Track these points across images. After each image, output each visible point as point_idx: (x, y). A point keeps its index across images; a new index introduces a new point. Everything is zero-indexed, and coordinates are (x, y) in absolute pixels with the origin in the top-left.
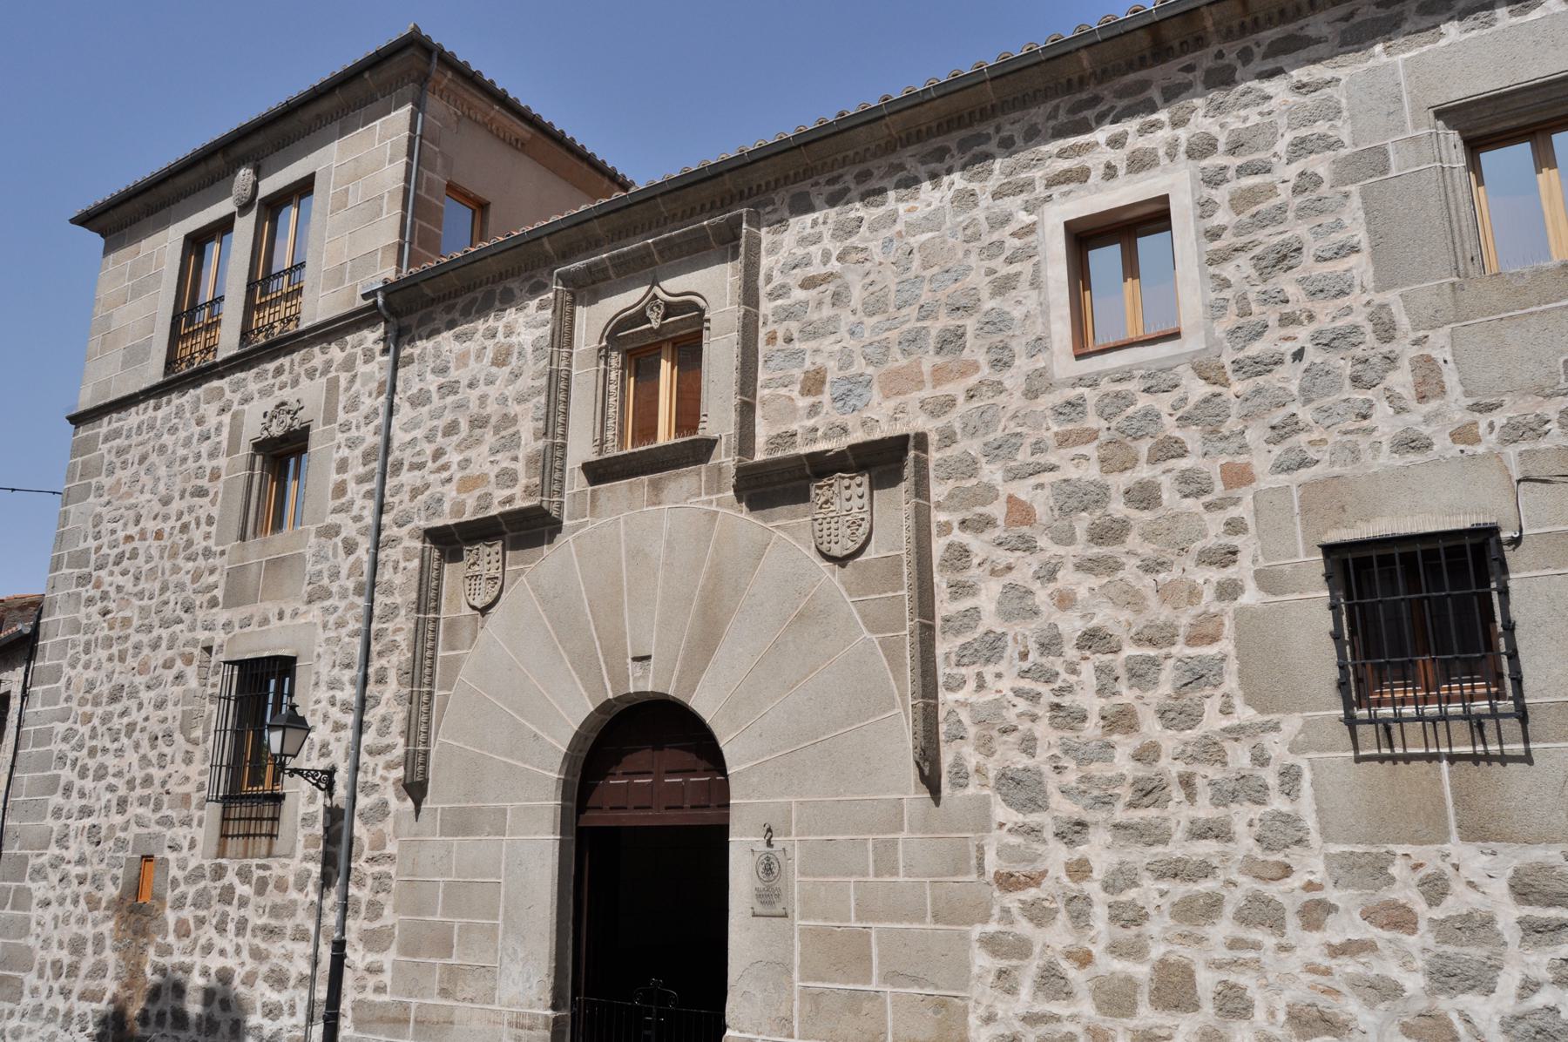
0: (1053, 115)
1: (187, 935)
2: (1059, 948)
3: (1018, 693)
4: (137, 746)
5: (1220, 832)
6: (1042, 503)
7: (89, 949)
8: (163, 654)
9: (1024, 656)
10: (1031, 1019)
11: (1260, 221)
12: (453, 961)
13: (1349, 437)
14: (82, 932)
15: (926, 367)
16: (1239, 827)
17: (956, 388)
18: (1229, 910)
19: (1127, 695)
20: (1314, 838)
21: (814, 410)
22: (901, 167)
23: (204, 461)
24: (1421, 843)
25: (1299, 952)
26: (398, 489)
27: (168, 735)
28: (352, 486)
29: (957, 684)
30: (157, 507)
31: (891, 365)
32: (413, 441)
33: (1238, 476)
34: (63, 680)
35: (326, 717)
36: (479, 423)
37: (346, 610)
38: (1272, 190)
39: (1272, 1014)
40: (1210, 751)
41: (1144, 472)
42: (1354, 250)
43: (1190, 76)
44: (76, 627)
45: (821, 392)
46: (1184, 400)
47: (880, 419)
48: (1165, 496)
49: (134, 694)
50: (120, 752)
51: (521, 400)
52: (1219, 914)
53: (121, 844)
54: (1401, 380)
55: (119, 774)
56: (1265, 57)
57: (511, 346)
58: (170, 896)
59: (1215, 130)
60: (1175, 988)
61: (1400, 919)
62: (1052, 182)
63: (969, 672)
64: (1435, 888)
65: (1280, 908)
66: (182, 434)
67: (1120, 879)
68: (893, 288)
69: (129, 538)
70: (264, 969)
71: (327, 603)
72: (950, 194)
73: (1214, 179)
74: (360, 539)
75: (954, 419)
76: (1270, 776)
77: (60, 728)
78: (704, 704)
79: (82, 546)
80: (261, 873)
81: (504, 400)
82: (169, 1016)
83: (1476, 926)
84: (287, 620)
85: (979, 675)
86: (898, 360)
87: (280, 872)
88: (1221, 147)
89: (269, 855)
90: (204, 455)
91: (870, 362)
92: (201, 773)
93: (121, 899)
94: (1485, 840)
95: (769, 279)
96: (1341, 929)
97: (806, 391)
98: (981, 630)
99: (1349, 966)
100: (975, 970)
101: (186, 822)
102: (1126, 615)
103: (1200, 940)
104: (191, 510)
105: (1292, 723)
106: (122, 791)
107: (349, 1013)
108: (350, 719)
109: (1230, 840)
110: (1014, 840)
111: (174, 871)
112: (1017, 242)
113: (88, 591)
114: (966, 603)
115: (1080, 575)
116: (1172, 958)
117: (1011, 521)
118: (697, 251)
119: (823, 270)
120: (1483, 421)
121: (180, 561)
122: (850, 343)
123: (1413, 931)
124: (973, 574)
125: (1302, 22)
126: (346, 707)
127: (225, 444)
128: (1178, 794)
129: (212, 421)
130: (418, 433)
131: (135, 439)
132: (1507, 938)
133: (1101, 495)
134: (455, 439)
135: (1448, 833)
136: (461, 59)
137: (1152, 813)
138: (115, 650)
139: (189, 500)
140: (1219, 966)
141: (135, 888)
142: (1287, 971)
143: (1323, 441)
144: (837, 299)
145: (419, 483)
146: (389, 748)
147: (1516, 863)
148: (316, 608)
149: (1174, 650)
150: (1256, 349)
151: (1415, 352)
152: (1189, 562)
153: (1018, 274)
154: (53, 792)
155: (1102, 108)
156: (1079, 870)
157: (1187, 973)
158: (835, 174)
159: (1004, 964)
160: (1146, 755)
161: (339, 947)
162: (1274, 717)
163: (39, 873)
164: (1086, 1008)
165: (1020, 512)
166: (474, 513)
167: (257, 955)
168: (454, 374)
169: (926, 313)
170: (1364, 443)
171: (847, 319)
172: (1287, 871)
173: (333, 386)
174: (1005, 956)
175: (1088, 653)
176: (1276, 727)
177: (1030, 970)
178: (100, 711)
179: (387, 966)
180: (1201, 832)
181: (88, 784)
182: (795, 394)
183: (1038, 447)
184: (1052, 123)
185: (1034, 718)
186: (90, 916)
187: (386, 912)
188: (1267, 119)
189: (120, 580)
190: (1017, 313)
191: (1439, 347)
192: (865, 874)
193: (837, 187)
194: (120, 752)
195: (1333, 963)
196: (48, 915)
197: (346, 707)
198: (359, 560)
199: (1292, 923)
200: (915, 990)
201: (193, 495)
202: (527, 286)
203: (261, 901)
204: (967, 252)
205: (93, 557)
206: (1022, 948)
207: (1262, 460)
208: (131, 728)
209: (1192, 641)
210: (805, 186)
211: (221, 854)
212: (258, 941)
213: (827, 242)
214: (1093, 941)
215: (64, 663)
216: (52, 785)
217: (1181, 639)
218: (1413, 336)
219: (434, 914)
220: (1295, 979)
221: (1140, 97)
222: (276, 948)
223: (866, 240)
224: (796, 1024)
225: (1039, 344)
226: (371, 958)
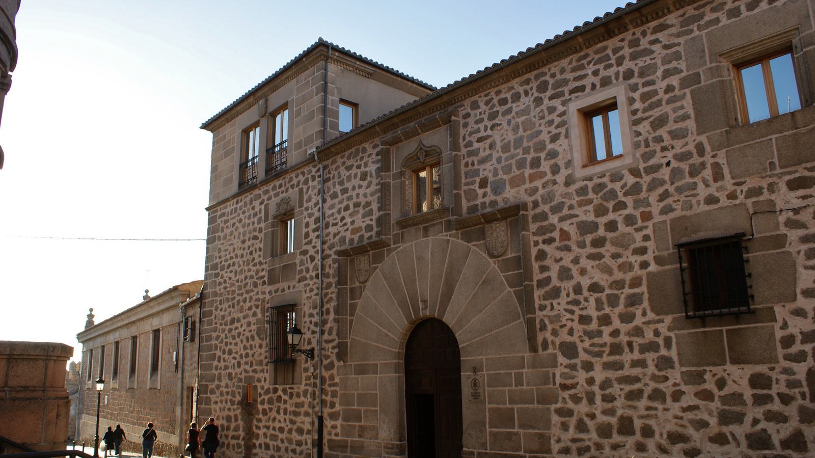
0: (570, 63)
1: (267, 414)
2: (583, 412)
3: (566, 310)
4: (242, 341)
5: (642, 363)
6: (573, 231)
7: (233, 420)
8: (248, 304)
9: (568, 295)
10: (574, 440)
11: (651, 107)
12: (362, 424)
13: (688, 198)
14: (230, 414)
15: (527, 175)
16: (650, 362)
17: (538, 183)
18: (646, 395)
19: (607, 310)
20: (677, 365)
21: (484, 195)
22: (513, 88)
23: (256, 225)
24: (716, 365)
25: (671, 411)
26: (328, 235)
27: (253, 337)
28: (311, 234)
29: (542, 308)
30: (240, 244)
31: (513, 174)
32: (333, 215)
33: (647, 216)
34: (213, 316)
35: (309, 329)
36: (357, 205)
37: (313, 285)
38: (655, 92)
39: (661, 435)
40: (638, 332)
41: (611, 216)
42: (688, 117)
43: (623, 44)
44: (215, 294)
45: (487, 187)
46: (625, 185)
47: (510, 195)
48: (619, 226)
49: (239, 320)
50: (236, 344)
51: (372, 195)
52: (642, 397)
53: (240, 380)
54: (708, 173)
55: (236, 353)
56: (652, 34)
57: (367, 172)
58: (259, 400)
59: (633, 67)
60: (626, 427)
61: (707, 396)
62: (572, 92)
63: (547, 303)
64: (721, 383)
65: (664, 394)
66: (247, 214)
67: (606, 384)
68: (512, 141)
69: (231, 258)
70: (295, 427)
71: (305, 282)
72: (532, 99)
73: (634, 88)
74: (316, 255)
75: (537, 196)
76: (660, 341)
77: (214, 335)
78: (449, 319)
79: (215, 262)
80: (291, 391)
81: (365, 195)
82: (263, 445)
83: (737, 398)
84: (291, 289)
85: (552, 304)
86: (516, 172)
87: (298, 390)
88: (636, 74)
89: (293, 383)
90: (256, 222)
91: (505, 173)
92: (266, 352)
93: (242, 400)
94: (739, 364)
95: (464, 139)
96: (686, 401)
97: (481, 187)
98: (551, 286)
99: (690, 415)
100: (553, 422)
101: (262, 371)
102: (606, 276)
103: (635, 408)
104: (253, 245)
105: (668, 319)
106: (238, 359)
107: (326, 444)
108: (318, 329)
109: (646, 367)
110: (566, 370)
111: (259, 390)
112: (559, 119)
113: (219, 280)
114: (545, 275)
115: (589, 261)
116: (625, 415)
117: (561, 240)
118: (432, 125)
119: (485, 134)
120: (739, 189)
121: (251, 267)
122: (496, 165)
123: (713, 401)
124: (548, 262)
125: (665, 18)
126: (316, 324)
127: (263, 218)
128: (627, 349)
129: (257, 209)
130: (335, 210)
131: (230, 217)
132: (748, 402)
133: (594, 227)
134: (348, 212)
135: (726, 362)
136: (340, 47)
137: (617, 357)
138: (230, 303)
139: (252, 242)
140: (642, 417)
141: (245, 397)
142: (666, 419)
143: (679, 201)
144: (491, 146)
145: (336, 231)
146: (333, 341)
147: (751, 372)
148: (302, 284)
149: (624, 291)
150: (652, 162)
151: (713, 160)
152: (629, 253)
153: (560, 133)
154: (214, 360)
155: (589, 59)
156: (590, 381)
157: (630, 420)
158: (487, 92)
159: (564, 419)
160: (615, 333)
161: (321, 419)
162: (661, 317)
163: (213, 392)
164: (594, 435)
165: (565, 235)
166: (358, 244)
167: (293, 422)
168: (347, 185)
169: (526, 151)
170: (694, 201)
171: (495, 155)
172: (667, 379)
173: (301, 191)
174: (564, 416)
175: (592, 293)
176: (663, 321)
177: (572, 422)
178: (228, 328)
179: (339, 426)
180: (635, 364)
181: (226, 356)
182: (477, 188)
183: (571, 207)
184: (570, 66)
185: (572, 320)
186: (232, 408)
187: (337, 405)
188: (653, 61)
189: (229, 275)
190: (560, 150)
191: (722, 159)
192: (512, 386)
193: (488, 98)
194: (236, 344)
195: (683, 414)
196: (217, 407)
197: (316, 324)
198: (316, 264)
199: (669, 399)
200: (531, 431)
201: (253, 239)
202: (372, 145)
203: (291, 401)
204: (540, 125)
205: (219, 266)
206: (570, 413)
207: (656, 208)
208: (239, 334)
209: (631, 287)
210: (476, 98)
211: (276, 383)
212: (292, 417)
213: (486, 122)
214: (596, 409)
215: (213, 309)
216: (213, 357)
217: (627, 286)
218: (712, 154)
219: (354, 406)
220: (670, 421)
221: (604, 54)
222: (299, 419)
223: (500, 120)
224: (488, 445)
225: (569, 164)
226: (333, 423)
